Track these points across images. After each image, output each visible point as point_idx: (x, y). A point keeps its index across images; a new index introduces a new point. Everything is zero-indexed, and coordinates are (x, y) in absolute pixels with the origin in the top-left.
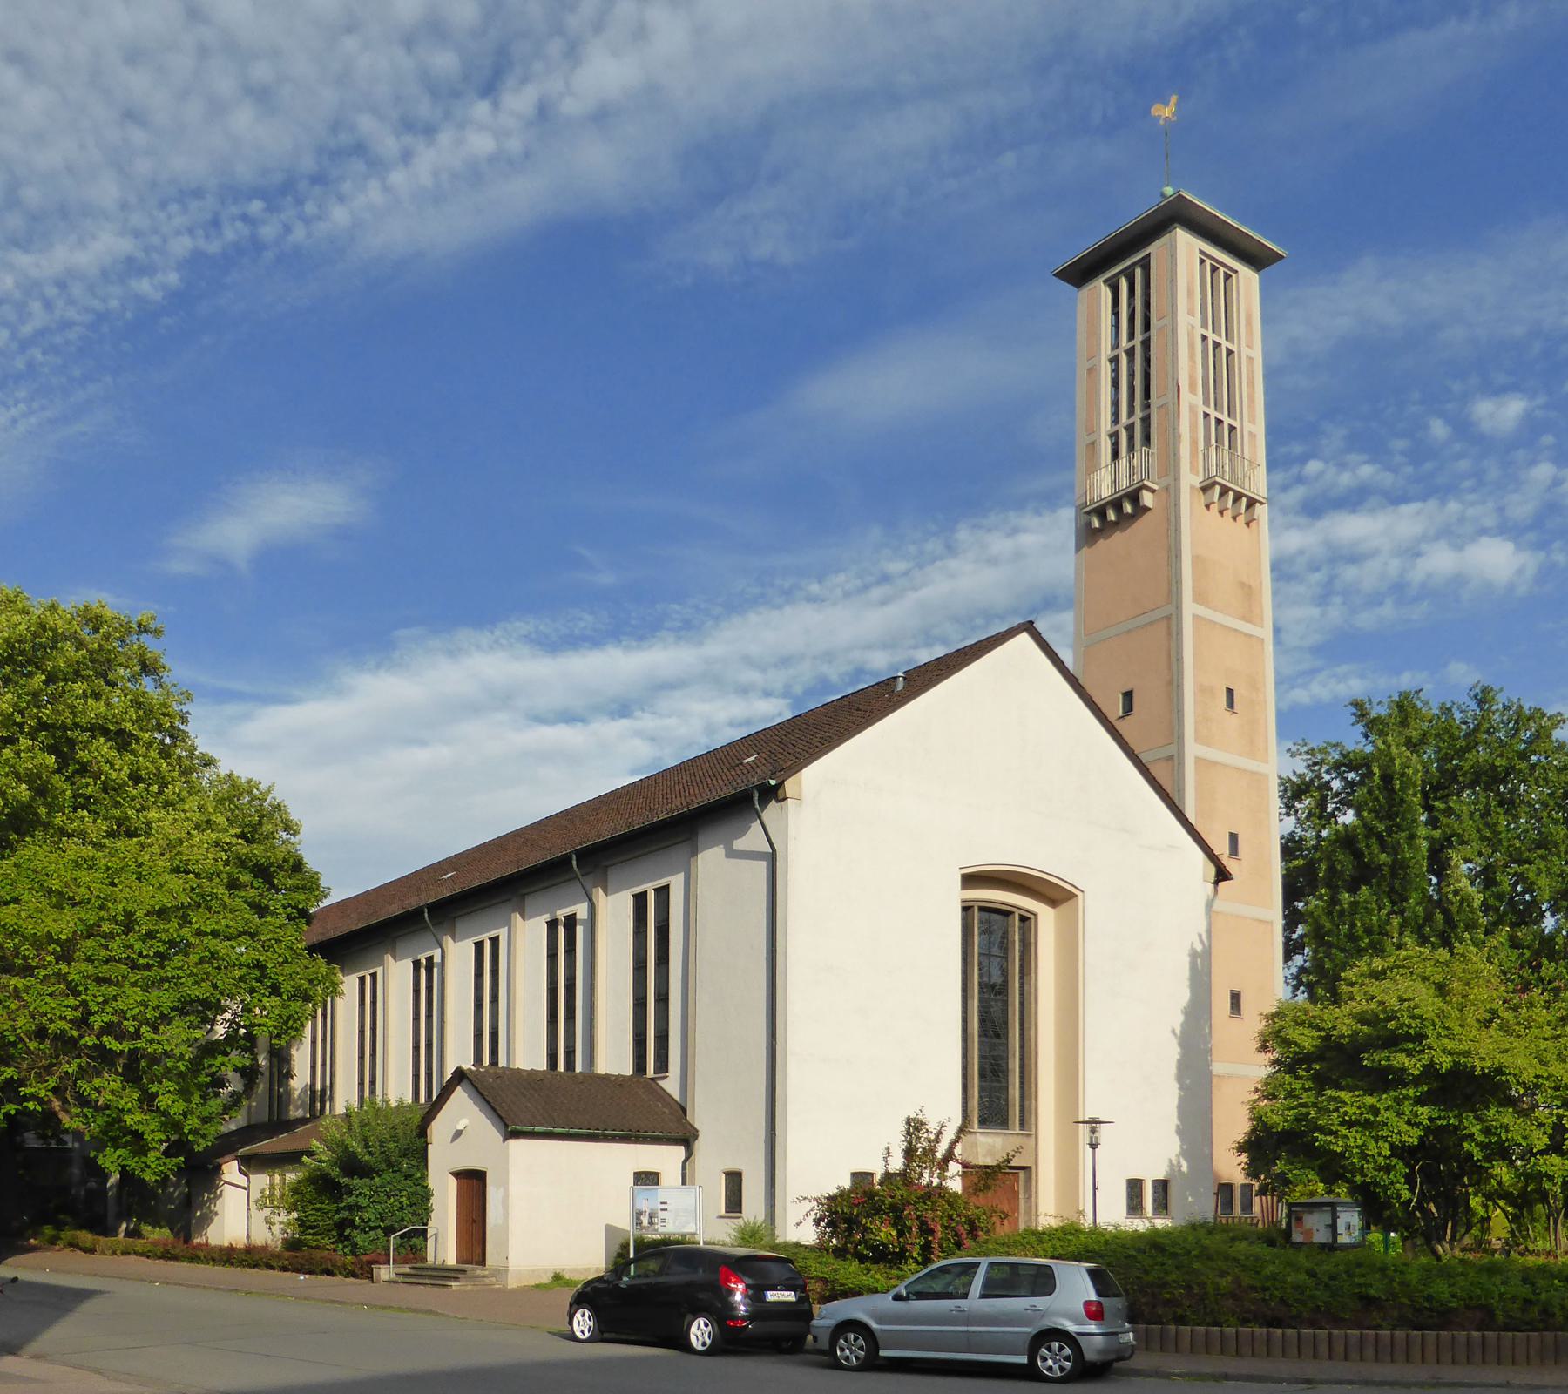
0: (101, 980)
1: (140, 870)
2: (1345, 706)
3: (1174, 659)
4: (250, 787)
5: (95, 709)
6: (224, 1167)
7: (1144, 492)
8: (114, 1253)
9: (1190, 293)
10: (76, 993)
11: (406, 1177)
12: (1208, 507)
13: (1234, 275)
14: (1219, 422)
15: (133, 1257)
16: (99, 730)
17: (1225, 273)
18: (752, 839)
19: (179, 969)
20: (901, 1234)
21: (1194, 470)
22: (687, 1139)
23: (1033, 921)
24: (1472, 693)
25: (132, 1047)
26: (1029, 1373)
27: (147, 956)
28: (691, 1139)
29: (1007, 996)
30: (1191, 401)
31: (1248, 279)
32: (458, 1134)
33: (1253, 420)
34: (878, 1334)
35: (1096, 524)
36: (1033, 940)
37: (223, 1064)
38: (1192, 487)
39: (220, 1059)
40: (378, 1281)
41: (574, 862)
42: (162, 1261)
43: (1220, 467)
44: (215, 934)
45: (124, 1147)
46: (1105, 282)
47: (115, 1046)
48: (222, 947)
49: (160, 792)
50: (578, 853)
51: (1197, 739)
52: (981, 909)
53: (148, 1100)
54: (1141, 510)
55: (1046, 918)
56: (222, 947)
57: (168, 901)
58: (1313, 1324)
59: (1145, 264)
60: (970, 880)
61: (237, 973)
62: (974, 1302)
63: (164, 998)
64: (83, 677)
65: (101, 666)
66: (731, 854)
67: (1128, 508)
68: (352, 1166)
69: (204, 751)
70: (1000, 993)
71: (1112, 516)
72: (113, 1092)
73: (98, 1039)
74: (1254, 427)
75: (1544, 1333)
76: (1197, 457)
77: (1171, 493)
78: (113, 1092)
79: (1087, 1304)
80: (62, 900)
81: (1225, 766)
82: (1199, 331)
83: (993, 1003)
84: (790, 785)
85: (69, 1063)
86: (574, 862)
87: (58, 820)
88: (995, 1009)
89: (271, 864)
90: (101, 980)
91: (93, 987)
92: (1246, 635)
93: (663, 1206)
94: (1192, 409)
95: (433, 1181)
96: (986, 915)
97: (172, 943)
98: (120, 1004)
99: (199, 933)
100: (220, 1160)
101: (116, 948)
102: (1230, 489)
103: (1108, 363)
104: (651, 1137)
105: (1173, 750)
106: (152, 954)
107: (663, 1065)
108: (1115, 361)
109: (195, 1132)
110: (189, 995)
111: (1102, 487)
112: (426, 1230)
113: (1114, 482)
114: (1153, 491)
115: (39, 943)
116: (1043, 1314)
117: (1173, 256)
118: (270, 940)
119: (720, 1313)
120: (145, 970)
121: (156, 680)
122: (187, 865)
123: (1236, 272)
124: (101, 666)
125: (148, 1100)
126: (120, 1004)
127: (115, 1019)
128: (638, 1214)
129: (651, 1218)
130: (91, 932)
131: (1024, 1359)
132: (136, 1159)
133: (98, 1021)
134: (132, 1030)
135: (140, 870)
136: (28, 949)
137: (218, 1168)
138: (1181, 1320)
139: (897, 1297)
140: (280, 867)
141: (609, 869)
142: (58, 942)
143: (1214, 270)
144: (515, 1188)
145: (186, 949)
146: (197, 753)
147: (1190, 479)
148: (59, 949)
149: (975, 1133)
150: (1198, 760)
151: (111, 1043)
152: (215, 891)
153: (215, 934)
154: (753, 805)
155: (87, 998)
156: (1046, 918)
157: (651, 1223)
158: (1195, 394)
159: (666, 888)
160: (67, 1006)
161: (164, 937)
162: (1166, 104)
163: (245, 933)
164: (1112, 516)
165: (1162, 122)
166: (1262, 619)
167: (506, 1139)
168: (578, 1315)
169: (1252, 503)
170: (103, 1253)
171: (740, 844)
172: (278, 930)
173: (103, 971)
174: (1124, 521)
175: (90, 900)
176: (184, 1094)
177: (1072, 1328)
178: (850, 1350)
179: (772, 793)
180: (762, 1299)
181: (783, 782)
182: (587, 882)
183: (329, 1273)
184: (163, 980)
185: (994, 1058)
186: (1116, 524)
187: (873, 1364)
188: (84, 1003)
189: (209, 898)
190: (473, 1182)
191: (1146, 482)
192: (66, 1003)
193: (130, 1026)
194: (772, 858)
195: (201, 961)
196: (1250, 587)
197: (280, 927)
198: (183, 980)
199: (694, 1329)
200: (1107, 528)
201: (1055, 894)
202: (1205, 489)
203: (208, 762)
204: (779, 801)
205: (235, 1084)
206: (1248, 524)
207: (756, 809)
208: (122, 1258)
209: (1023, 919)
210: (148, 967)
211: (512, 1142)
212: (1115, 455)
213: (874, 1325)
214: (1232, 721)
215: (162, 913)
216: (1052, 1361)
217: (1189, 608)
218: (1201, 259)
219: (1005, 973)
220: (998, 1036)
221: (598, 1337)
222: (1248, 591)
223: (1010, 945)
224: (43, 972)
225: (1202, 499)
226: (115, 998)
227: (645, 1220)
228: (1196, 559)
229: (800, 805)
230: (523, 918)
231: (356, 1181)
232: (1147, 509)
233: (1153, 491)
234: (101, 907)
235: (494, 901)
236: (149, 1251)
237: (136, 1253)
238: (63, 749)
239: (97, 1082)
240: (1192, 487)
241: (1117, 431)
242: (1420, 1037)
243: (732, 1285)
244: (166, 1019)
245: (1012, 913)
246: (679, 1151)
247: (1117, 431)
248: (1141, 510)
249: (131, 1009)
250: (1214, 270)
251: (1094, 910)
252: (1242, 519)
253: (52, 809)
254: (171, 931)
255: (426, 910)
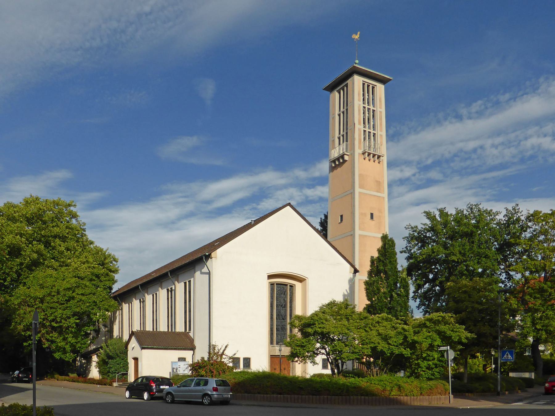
0: (51, 308)
1: (64, 277)
2: (422, 213)
3: (353, 205)
4: (101, 250)
5: (56, 230)
6: (93, 357)
7: (345, 156)
8: (62, 381)
9: (359, 94)
10: (44, 311)
11: (123, 359)
12: (365, 159)
13: (375, 87)
14: (369, 132)
15: (65, 381)
16: (55, 237)
17: (372, 86)
18: (205, 270)
19: (71, 304)
20: (206, 373)
21: (360, 148)
22: (193, 348)
23: (294, 287)
24: (468, 207)
25: (59, 325)
26: (202, 403)
27: (63, 301)
28: (194, 349)
29: (286, 308)
30: (359, 127)
31: (380, 88)
32: (133, 348)
33: (381, 130)
34: (174, 395)
35: (333, 165)
36: (294, 292)
37: (87, 329)
38: (359, 154)
39: (86, 328)
40: (113, 387)
41: (169, 274)
42: (72, 382)
43: (370, 147)
44: (82, 294)
45: (61, 352)
46: (337, 91)
47: (55, 325)
48: (84, 298)
49: (74, 253)
50: (170, 271)
51: (360, 229)
52: (277, 284)
53: (65, 339)
54: (345, 161)
55: (298, 286)
56: (84, 298)
57: (69, 286)
58: (288, 394)
59: (347, 85)
60: (270, 277)
61: (88, 304)
62: (192, 387)
63: (68, 312)
64: (54, 221)
65: (58, 217)
66: (202, 273)
67: (341, 161)
68: (110, 357)
69: (90, 240)
70: (284, 307)
71: (337, 163)
72: (55, 337)
73: (50, 323)
74: (381, 132)
75: (347, 397)
76: (361, 144)
77: (352, 156)
78: (55, 337)
79: (213, 388)
80: (42, 287)
81: (369, 236)
82: (362, 105)
83: (282, 310)
84: (213, 254)
85: (43, 330)
86: (169, 274)
87: (46, 262)
88: (282, 312)
89: (99, 274)
90: (51, 308)
91: (49, 310)
92: (378, 196)
93: (179, 367)
94: (359, 130)
95: (129, 361)
96: (277, 285)
97: (70, 297)
98: (56, 314)
99: (78, 294)
100: (92, 355)
101: (55, 299)
102: (371, 153)
103: (338, 116)
104: (183, 349)
105: (352, 233)
106: (64, 300)
107: (190, 329)
108: (339, 115)
109: (80, 347)
110: (74, 311)
111: (335, 153)
112: (127, 373)
113: (339, 152)
114: (348, 155)
115: (35, 298)
116: (204, 390)
117: (353, 84)
118: (98, 295)
119: (150, 391)
120: (63, 305)
121: (76, 220)
122: (78, 275)
123: (376, 86)
124: (58, 217)
125: (65, 339)
126: (56, 314)
127: (54, 318)
128: (173, 369)
129: (176, 370)
130: (49, 295)
131: (201, 400)
132: (63, 355)
133: (50, 318)
134: (59, 320)
135: (64, 277)
136: (32, 300)
137: (91, 357)
138: (259, 393)
139: (178, 387)
140: (102, 275)
141: (179, 275)
142: (39, 298)
143: (368, 86)
144: (143, 362)
145: (73, 298)
146: (88, 240)
147: (358, 151)
148: (40, 300)
149: (275, 346)
150: (360, 235)
151: (54, 324)
152: (83, 282)
153: (82, 294)
154: (203, 260)
155: (47, 313)
156: (298, 286)
157: (176, 371)
158: (361, 125)
159: (190, 281)
160: (42, 315)
161: (67, 295)
162: (357, 35)
163: (91, 293)
164: (337, 163)
165: (355, 40)
166: (384, 191)
167: (141, 350)
168: (127, 392)
169: (379, 157)
170: (60, 380)
171: (203, 271)
172: (101, 292)
173: (52, 305)
174: (341, 164)
175: (48, 286)
176: (76, 337)
177: (210, 393)
178: (169, 399)
179: (208, 257)
180: (159, 387)
181: (211, 254)
182: (173, 279)
183: (105, 385)
184: (67, 307)
185: (282, 325)
186: (339, 165)
187: (173, 402)
188: (46, 314)
189: (81, 284)
190: (136, 359)
191: (345, 153)
192: (41, 314)
193: (59, 320)
194: (209, 273)
195: (78, 302)
196: (380, 182)
197: (102, 291)
198: (73, 307)
199: (145, 395)
200: (336, 167)
201: (301, 280)
202: (363, 154)
203: (92, 243)
204: (211, 259)
205: (93, 334)
206: (379, 163)
207: (204, 261)
208: (64, 381)
209: (290, 286)
210: (63, 304)
211: (143, 350)
212: (339, 144)
213: (173, 393)
214: (372, 223)
215: (69, 289)
216: (206, 401)
217: (357, 190)
218: (363, 83)
219: (285, 301)
220: (283, 319)
221: (130, 397)
222: (379, 184)
223: (287, 294)
224: (36, 306)
225: (363, 157)
226: (55, 312)
227: (175, 370)
228: (360, 175)
229: (216, 259)
230: (178, 283)
231: (110, 361)
232: (346, 161)
233: (348, 155)
234: (52, 288)
235: (154, 284)
236: (69, 380)
237: (67, 380)
238: (47, 244)
239: (51, 335)
240: (359, 154)
241: (340, 137)
242: (314, 324)
243: (152, 384)
244: (69, 318)
245: (287, 285)
246: (192, 352)
247: (340, 137)
248: (345, 161)
249: (59, 315)
250: (368, 86)
251: (310, 283)
252: (377, 161)
253: (44, 260)
254: (70, 294)
255: (140, 286)
